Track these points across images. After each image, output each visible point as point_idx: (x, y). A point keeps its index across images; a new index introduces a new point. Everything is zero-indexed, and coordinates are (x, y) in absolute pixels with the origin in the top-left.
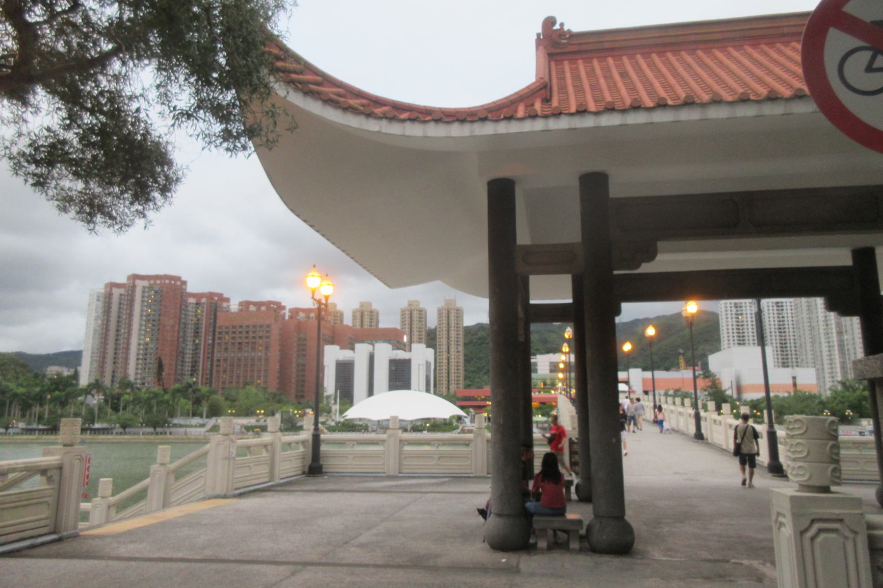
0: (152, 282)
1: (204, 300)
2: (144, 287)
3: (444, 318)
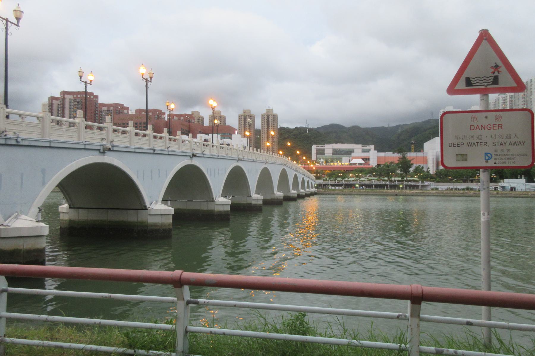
0: (75, 96)
1: (112, 108)
2: (70, 99)
3: (265, 121)
